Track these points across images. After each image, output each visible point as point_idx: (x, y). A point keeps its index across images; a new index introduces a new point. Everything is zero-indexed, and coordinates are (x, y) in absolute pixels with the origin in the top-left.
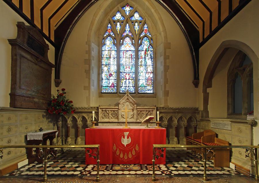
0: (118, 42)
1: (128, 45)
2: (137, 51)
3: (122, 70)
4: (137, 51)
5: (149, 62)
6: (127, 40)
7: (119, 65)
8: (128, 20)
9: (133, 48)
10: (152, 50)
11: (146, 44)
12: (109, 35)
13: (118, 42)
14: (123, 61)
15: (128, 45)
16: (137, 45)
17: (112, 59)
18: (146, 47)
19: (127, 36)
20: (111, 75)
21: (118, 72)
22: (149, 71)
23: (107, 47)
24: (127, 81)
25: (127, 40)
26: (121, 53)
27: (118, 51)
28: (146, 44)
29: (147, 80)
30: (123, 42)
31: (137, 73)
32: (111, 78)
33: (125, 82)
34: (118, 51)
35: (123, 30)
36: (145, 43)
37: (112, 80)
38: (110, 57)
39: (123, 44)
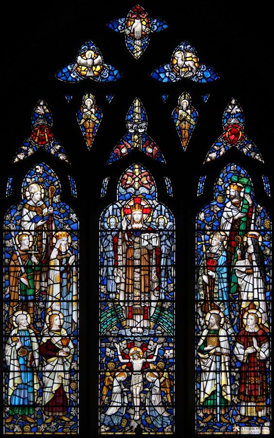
0: (87, 190)
1: (138, 211)
2: (186, 236)
3: (106, 322)
4: (186, 236)
5: (252, 287)
6: (137, 180)
7: (90, 301)
8: (136, 78)
9: (165, 221)
10: (267, 223)
11: (233, 200)
12: (42, 156)
13: (87, 190)
14: (115, 282)
15: (138, 211)
16: (186, 200)
17: (54, 274)
18: (231, 213)
19: (136, 157)
20: (48, 351)
21: (88, 336)
22: (251, 326)
23: (27, 215)
24: (137, 379)
25: (137, 180)
26: (106, 246)
27: (88, 239)
28: (233, 200)
29: (242, 371)
30: (112, 188)
31: (186, 339)
32: (53, 363)
33: (127, 383)
34: (88, 239)
35: (113, 126)
36: (232, 191)
37: (57, 376)
38: (45, 264)
39: (111, 198)
